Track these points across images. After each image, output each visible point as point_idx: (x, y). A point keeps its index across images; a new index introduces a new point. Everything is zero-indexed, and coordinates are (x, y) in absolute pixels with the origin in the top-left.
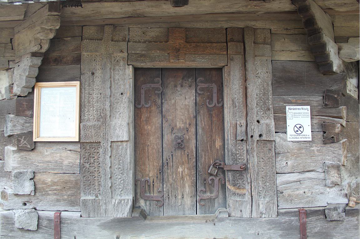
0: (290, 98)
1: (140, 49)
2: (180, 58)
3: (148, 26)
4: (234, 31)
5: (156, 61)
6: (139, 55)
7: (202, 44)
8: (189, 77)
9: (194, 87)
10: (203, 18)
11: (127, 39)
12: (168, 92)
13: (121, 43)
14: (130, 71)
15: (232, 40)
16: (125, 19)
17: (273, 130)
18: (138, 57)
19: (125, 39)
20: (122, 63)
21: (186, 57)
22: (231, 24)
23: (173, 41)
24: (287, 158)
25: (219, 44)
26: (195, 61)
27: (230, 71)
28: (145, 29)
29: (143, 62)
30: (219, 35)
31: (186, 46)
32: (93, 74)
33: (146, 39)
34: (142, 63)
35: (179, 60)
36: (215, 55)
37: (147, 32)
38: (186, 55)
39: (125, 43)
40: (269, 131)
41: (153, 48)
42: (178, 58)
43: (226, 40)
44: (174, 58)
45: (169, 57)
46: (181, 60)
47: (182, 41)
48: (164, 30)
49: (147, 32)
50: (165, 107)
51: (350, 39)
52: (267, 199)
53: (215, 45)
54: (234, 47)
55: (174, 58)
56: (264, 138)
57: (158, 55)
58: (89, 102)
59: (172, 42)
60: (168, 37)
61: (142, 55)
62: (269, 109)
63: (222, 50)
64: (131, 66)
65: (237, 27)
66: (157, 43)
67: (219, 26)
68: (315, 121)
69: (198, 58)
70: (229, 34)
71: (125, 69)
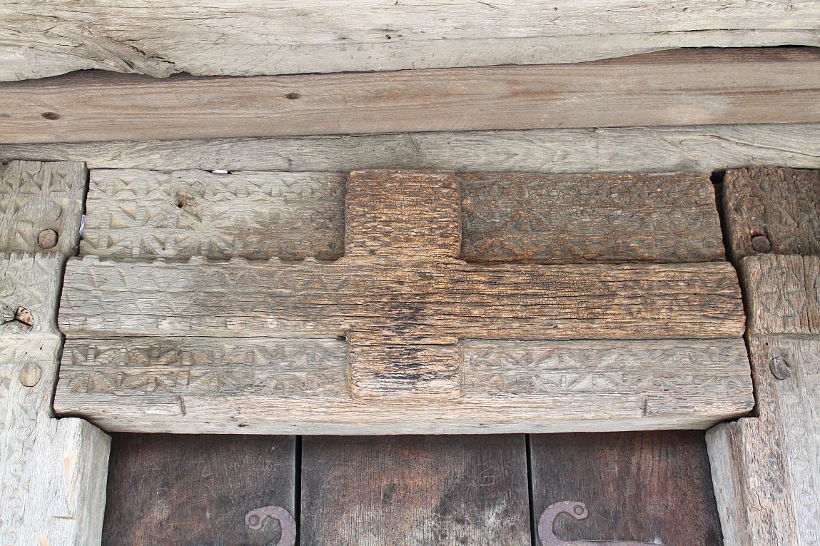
1: (143, 304)
2: (423, 370)
3: (214, 156)
4: (766, 185)
5: (258, 389)
6: (138, 344)
7: (573, 273)
8: (483, 500)
10: (574, 100)
11: (67, 241)
13: (18, 263)
15: (764, 244)
16: (50, 98)
18: (130, 362)
19: (52, 235)
21: (467, 357)
22: (744, 149)
23: (372, 252)
25: (688, 270)
26: (530, 389)
27: (779, 456)
28: (192, 177)
29: (155, 391)
30: (678, 215)
31: (465, 286)
33: (189, 238)
34: (152, 403)
35: (420, 384)
36: (667, 345)
37: (202, 195)
38: (467, 343)
39: (49, 265)
41: (232, 297)
42: (406, 366)
43: (726, 241)
44: (381, 367)
45: (348, 360)
46: (434, 384)
47: (438, 251)
48: (315, 186)
49: (202, 195)
53: (660, 273)
54: (791, 288)
55: (381, 367)
57: (270, 345)
59: (371, 260)
60: (341, 229)
61: (158, 350)
63: (715, 308)
64: (75, 422)
65: (781, 163)
66: (260, 266)
67: (671, 159)
69: (551, 363)
70: (738, 210)
71: (28, 445)
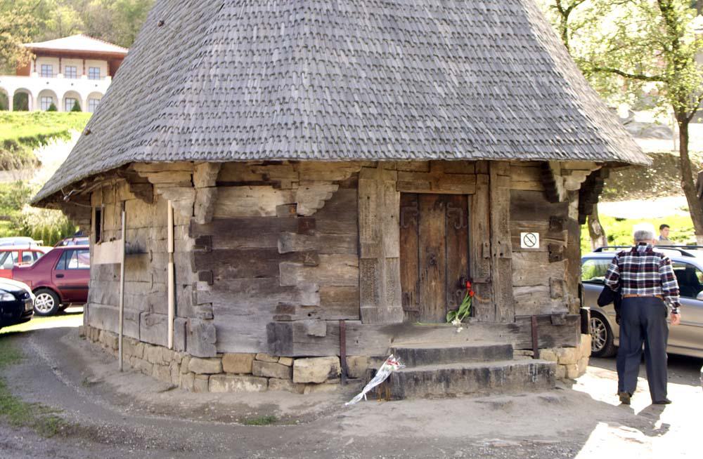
0: (524, 223)
9: (444, 210)
12: (423, 214)
14: (398, 196)
15: (480, 172)
17: (511, 249)
20: (392, 189)
24: (521, 274)
32: (368, 198)
40: (508, 250)
50: (421, 227)
51: (574, 172)
52: (506, 308)
56: (504, 256)
58: (366, 223)
61: (408, 183)
62: (507, 232)
68: (543, 243)
